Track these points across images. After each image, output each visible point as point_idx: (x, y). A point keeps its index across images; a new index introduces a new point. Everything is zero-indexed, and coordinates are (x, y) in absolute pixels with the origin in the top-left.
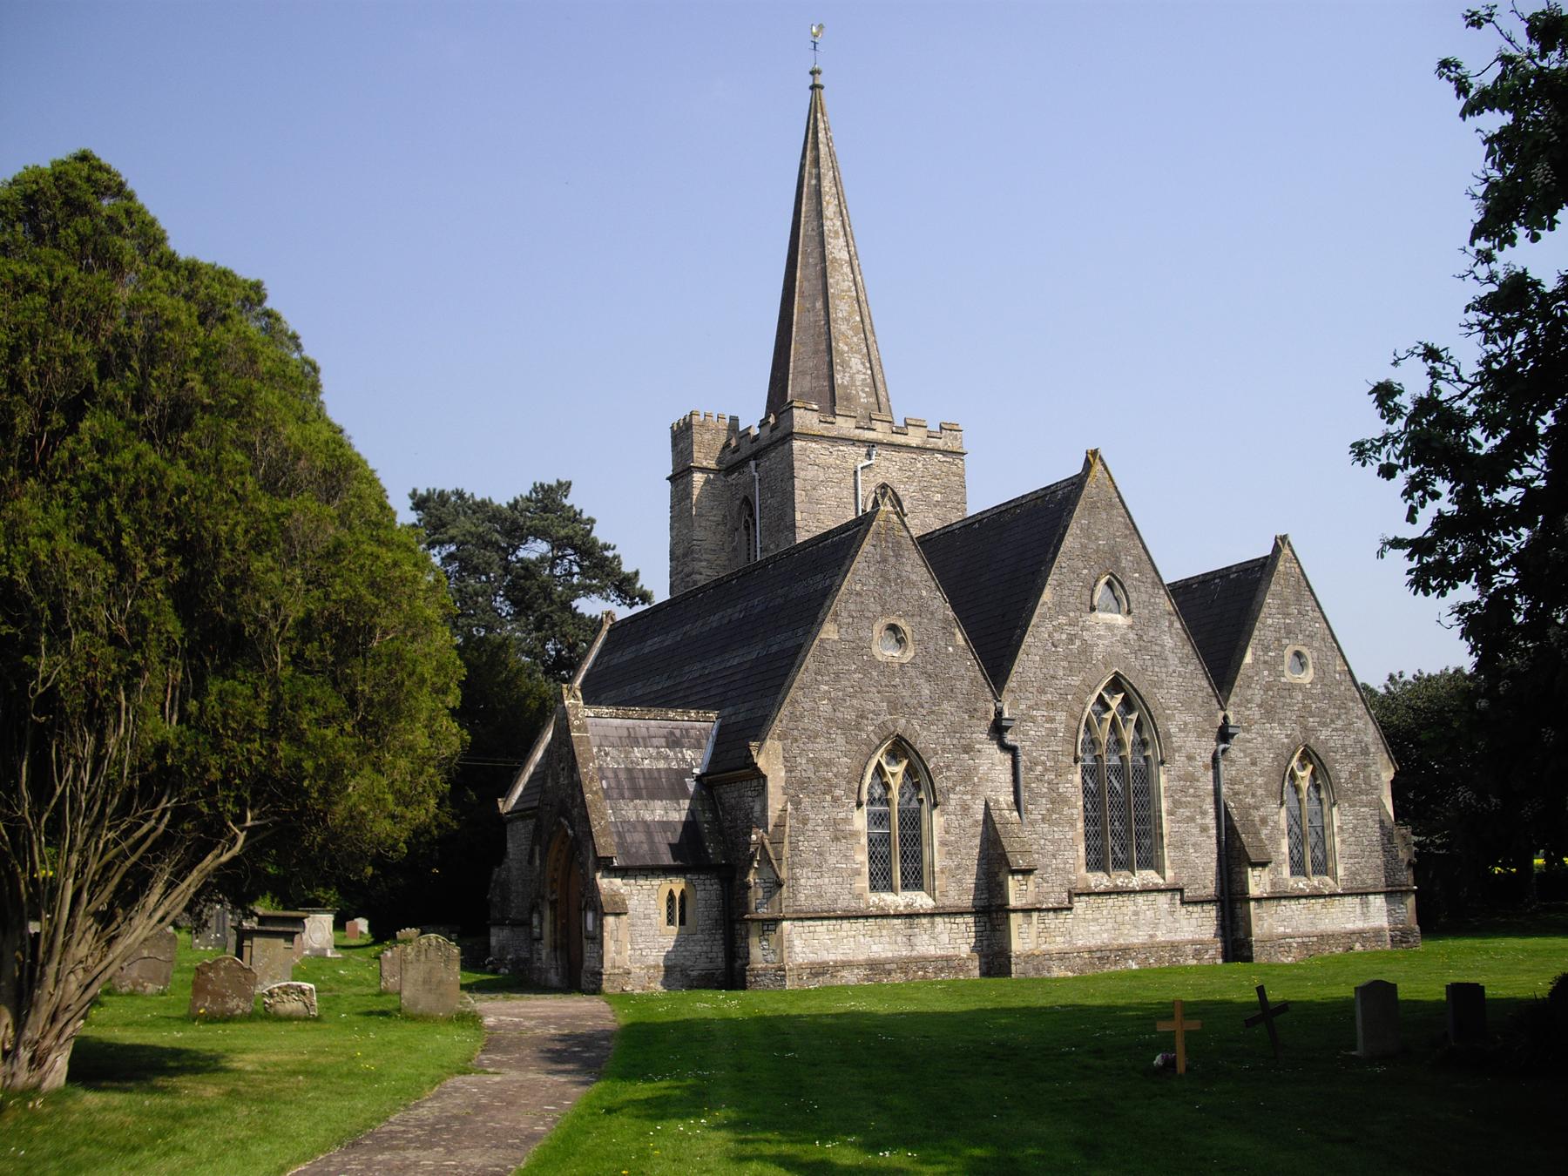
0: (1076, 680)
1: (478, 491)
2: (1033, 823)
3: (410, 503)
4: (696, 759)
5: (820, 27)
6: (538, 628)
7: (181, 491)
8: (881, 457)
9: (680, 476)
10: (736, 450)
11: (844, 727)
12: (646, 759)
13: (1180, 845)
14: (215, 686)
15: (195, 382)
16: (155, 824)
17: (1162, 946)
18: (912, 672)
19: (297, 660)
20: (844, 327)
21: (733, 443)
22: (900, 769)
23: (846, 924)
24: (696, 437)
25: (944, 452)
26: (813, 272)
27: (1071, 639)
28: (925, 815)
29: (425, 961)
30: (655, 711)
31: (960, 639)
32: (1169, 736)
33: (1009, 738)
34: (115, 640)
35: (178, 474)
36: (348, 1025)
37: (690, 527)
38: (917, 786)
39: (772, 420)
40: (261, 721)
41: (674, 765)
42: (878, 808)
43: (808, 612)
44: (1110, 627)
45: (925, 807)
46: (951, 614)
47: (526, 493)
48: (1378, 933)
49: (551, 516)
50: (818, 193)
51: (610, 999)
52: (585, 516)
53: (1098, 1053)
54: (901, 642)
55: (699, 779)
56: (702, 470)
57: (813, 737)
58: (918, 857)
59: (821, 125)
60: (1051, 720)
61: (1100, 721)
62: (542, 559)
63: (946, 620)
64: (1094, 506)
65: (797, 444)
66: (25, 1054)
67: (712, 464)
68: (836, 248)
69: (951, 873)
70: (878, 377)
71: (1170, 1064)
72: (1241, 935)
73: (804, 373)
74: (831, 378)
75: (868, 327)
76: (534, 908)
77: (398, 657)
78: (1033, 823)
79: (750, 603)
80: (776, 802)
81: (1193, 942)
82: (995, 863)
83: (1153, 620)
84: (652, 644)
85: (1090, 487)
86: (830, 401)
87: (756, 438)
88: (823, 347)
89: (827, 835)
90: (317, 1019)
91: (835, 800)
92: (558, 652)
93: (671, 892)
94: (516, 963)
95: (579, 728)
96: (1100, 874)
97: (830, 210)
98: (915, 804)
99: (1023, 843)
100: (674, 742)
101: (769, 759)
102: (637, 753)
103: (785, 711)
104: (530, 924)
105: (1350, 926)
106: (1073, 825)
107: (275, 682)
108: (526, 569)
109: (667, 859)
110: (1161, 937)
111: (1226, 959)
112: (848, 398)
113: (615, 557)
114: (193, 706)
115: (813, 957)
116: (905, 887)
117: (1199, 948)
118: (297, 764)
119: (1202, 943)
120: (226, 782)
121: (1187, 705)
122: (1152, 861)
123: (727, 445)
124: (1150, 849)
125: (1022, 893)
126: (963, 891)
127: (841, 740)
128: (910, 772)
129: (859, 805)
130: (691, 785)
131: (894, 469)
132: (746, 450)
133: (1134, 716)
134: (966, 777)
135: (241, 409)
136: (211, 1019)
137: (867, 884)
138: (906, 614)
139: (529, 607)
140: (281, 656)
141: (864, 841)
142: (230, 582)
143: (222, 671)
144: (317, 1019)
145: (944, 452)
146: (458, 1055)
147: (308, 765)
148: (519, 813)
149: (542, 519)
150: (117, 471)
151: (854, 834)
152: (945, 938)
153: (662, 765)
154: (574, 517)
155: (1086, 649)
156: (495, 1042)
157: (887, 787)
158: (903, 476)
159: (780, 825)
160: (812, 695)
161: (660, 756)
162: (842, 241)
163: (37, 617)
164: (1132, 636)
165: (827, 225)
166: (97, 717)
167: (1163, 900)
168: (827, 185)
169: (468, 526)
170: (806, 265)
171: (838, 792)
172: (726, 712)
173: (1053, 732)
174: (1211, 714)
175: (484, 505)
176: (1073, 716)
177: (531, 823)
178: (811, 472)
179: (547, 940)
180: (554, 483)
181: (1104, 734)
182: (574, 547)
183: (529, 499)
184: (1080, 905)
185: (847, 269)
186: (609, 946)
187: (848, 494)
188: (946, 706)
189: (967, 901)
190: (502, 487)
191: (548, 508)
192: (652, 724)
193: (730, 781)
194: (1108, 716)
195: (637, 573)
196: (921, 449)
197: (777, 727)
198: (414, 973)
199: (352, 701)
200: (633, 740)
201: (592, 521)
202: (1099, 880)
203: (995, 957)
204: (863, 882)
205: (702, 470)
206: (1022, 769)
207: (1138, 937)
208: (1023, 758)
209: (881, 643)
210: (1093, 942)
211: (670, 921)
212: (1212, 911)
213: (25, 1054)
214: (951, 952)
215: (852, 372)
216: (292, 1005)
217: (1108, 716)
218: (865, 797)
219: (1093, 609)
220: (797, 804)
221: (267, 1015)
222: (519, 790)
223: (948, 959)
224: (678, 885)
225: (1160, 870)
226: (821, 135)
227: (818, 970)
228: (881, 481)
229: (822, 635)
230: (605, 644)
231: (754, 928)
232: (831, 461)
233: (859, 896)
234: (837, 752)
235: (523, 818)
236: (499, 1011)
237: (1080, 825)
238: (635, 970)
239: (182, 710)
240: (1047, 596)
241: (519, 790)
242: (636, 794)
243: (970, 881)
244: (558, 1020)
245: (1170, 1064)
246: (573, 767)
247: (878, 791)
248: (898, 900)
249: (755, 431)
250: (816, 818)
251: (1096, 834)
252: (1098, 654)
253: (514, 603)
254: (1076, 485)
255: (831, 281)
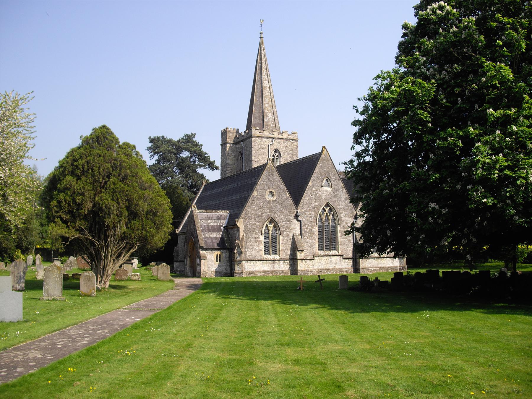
0: (317, 204)
1: (169, 136)
2: (305, 239)
3: (149, 140)
4: (224, 222)
5: (263, 20)
6: (186, 178)
7: (127, 191)
8: (276, 142)
9: (223, 145)
10: (238, 138)
11: (258, 216)
12: (211, 223)
13: (343, 245)
14: (133, 222)
15: (129, 172)
16: (123, 245)
17: (337, 269)
18: (275, 203)
19: (146, 218)
20: (267, 106)
21: (237, 136)
22: (272, 226)
23: (324, 258)
24: (228, 135)
25: (292, 140)
26: (259, 90)
27: (316, 194)
28: (278, 236)
29: (162, 270)
30: (214, 211)
31: (288, 194)
32: (341, 218)
33: (299, 218)
34: (117, 215)
35: (126, 188)
36: (147, 282)
37: (226, 159)
38: (276, 230)
39: (247, 131)
40: (140, 228)
41: (218, 224)
42: (266, 235)
43: (251, 187)
44: (326, 191)
45: (278, 235)
46: (285, 188)
47: (182, 137)
48: (396, 267)
49: (189, 144)
50: (261, 68)
51: (202, 278)
52: (199, 144)
53: (291, 287)
54: (273, 195)
55: (224, 227)
56: (229, 143)
57: (251, 218)
58: (276, 247)
59: (262, 48)
60: (310, 214)
61: (323, 214)
62: (187, 157)
63: (284, 190)
64: (323, 161)
65: (253, 139)
66: (103, 282)
67: (232, 142)
68: (266, 84)
69: (284, 251)
70: (276, 119)
71: (300, 289)
72: (358, 267)
73: (256, 118)
74: (263, 120)
75: (274, 105)
76: (185, 257)
77: (163, 216)
78: (305, 239)
79: (237, 187)
80: (241, 233)
81: (346, 268)
82: (294, 248)
83: (338, 189)
84: (215, 191)
85: (323, 156)
86: (263, 126)
87: (243, 136)
88: (261, 111)
89: (254, 241)
90: (141, 281)
91: (256, 233)
92: (192, 183)
93: (217, 255)
94: (180, 271)
95: (196, 215)
96: (322, 251)
97: (264, 73)
98: (275, 234)
99: (302, 244)
100: (219, 218)
101: (240, 223)
102: (210, 221)
103: (244, 212)
104: (184, 261)
105: (388, 266)
106: (315, 239)
107: (142, 221)
108: (182, 160)
109: (216, 247)
110: (337, 267)
111: (354, 272)
112: (267, 125)
113: (208, 156)
114: (129, 226)
115: (250, 270)
116: (273, 254)
117: (347, 270)
118: (146, 235)
119: (348, 268)
120: (135, 238)
121: (346, 210)
122: (335, 248)
123: (236, 137)
124: (335, 246)
125: (301, 256)
126: (287, 255)
127: (257, 219)
128: (275, 227)
129: (262, 234)
130: (222, 229)
131: (279, 145)
132: (241, 139)
133: (332, 213)
134: (288, 228)
135: (136, 175)
136: (119, 280)
137: (263, 253)
138: (274, 189)
139: (183, 171)
140: (143, 217)
141: (263, 243)
142: (135, 205)
143: (133, 219)
144: (141, 281)
145: (292, 140)
146: (170, 287)
147: (148, 235)
148: (181, 233)
149: (187, 145)
150: (117, 188)
151: (260, 241)
152: (282, 266)
153: (215, 224)
154: (197, 145)
155: (320, 196)
156: (177, 285)
157: (269, 230)
158: (281, 146)
159: (242, 239)
160: (251, 208)
161: (215, 222)
162: (267, 82)
163: (106, 213)
164: (332, 193)
165: (263, 77)
166: (114, 228)
167: (338, 258)
168: (263, 65)
169: (166, 148)
170: (257, 88)
171: (256, 231)
172: (231, 211)
173: (311, 217)
174: (353, 212)
175: (170, 140)
176: (316, 213)
177: (184, 236)
178: (257, 146)
179: (188, 265)
180: (190, 134)
181: (324, 217)
182: (196, 154)
183: (183, 139)
184: (316, 258)
185: (268, 90)
186: (202, 266)
187: (266, 152)
188: (283, 210)
189: (288, 257)
190: (176, 136)
191: (189, 141)
192: (213, 214)
193: (232, 228)
194: (325, 213)
195: (214, 161)
196: (286, 139)
197: (242, 216)
198: (160, 271)
199: (155, 224)
200: (209, 218)
201: (202, 145)
202: (322, 253)
203: (294, 270)
204: (263, 252)
205: (229, 143)
206: (302, 226)
207: (331, 267)
208: (303, 224)
209: (269, 194)
210: (320, 268)
211: (217, 261)
212: (351, 261)
213: (103, 282)
214: (283, 269)
215: (269, 118)
216: (135, 278)
217: (325, 213)
218: (263, 232)
219: (322, 186)
220: (246, 234)
221: (130, 280)
222: (181, 227)
223: (283, 271)
224: (219, 253)
225: (338, 251)
226: (262, 51)
227: (251, 273)
228: (275, 148)
229: (253, 194)
230: (203, 189)
231: (236, 263)
232: (262, 143)
233: (261, 256)
234: (256, 222)
235: (182, 234)
236: (178, 280)
237: (317, 239)
238: (209, 272)
239: (127, 226)
240: (310, 183)
241: (181, 227)
242: (209, 231)
243: (289, 252)
244: (190, 282)
245: (300, 289)
246: (194, 224)
247: (267, 231)
248: (271, 257)
249: (243, 134)
250: (251, 237)
251: (322, 242)
252: (323, 198)
253: (179, 169)
254: (320, 154)
255: (264, 93)
